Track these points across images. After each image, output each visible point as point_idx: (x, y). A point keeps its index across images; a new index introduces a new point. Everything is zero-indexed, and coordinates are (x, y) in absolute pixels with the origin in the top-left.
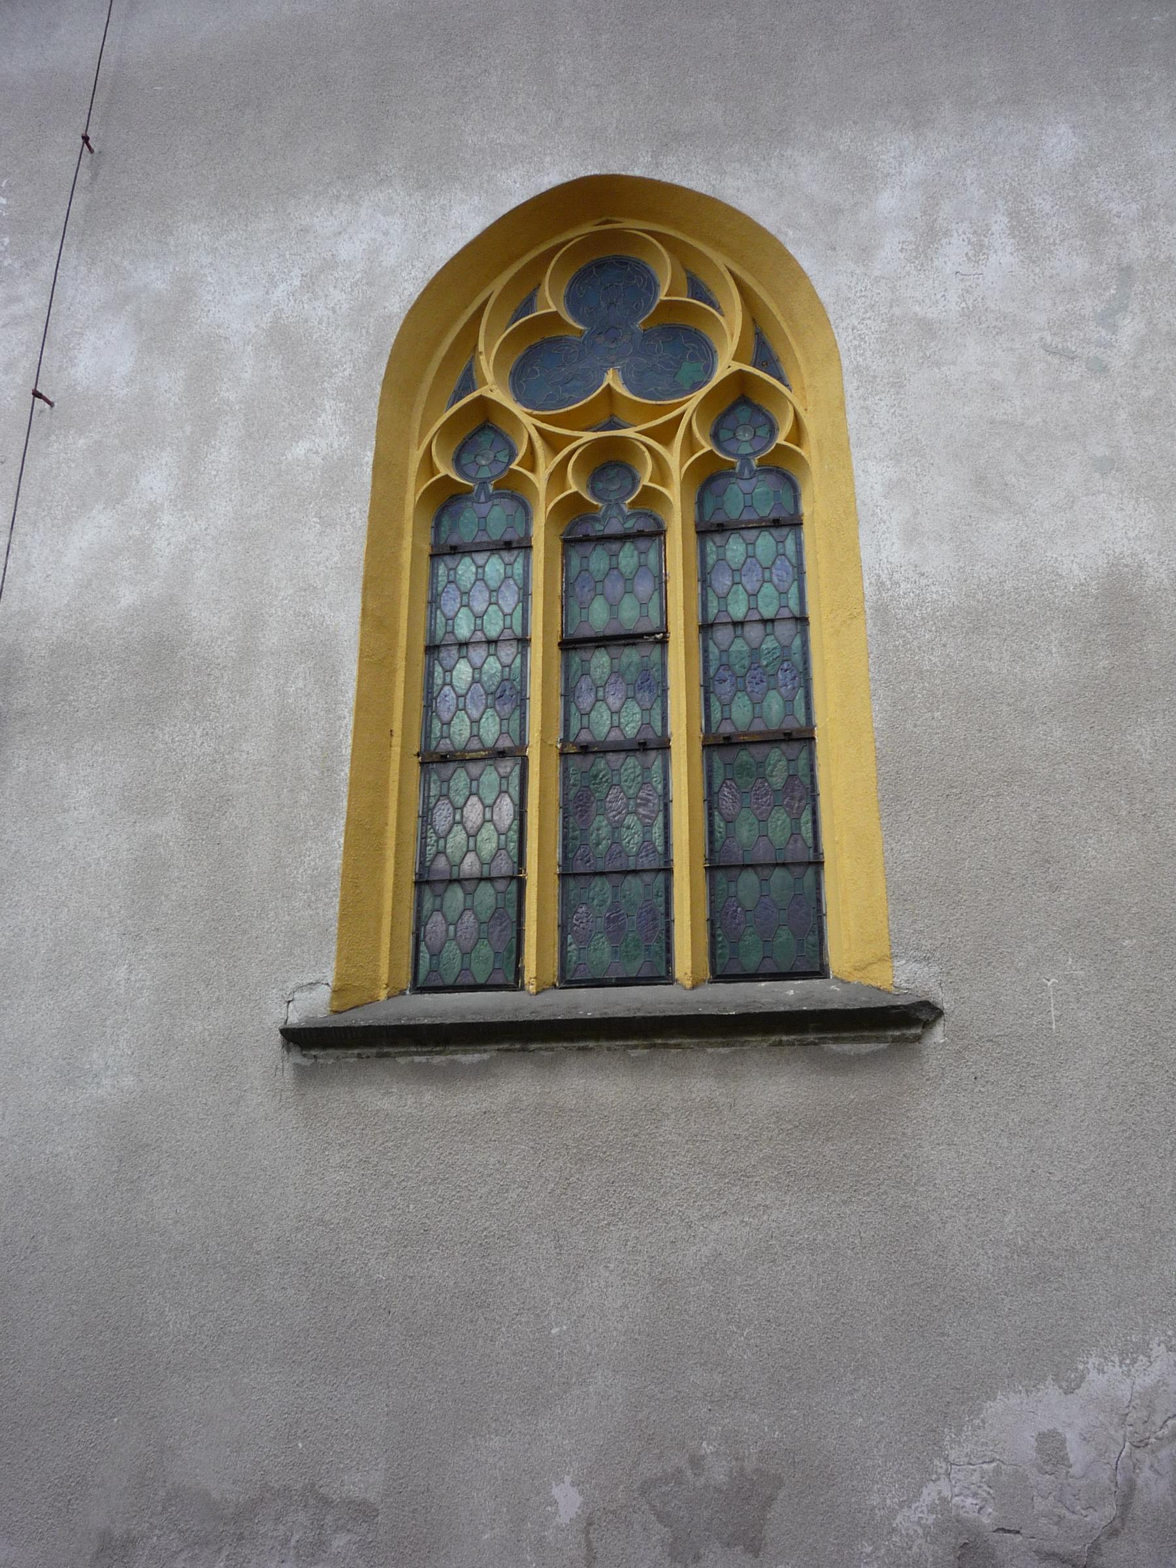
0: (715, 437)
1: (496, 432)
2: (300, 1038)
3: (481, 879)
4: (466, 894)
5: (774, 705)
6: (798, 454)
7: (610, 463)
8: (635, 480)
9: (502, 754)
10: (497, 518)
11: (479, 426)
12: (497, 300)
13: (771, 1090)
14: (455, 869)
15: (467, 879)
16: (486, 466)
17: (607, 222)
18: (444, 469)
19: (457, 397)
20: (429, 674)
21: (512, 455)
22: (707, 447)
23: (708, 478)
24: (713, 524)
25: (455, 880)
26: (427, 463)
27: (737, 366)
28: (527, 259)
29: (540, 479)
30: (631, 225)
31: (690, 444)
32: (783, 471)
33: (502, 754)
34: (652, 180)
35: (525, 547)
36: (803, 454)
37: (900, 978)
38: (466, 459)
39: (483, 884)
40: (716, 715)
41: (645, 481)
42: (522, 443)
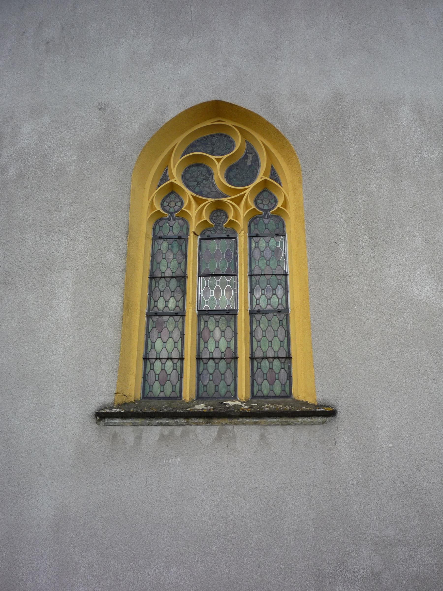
0: (256, 203)
1: (269, 192)
2: (102, 416)
3: (275, 358)
4: (270, 363)
5: (172, 304)
6: (285, 212)
7: (219, 210)
9: (177, 314)
11: (172, 192)
13: (282, 437)
14: (158, 355)
15: (216, 358)
16: (173, 207)
17: (219, 121)
18: (158, 208)
22: (253, 207)
23: (253, 219)
25: (276, 358)
27: (264, 178)
30: (229, 123)
31: (247, 206)
33: (279, 312)
34: (242, 108)
36: (287, 211)
39: (222, 360)
40: (254, 303)
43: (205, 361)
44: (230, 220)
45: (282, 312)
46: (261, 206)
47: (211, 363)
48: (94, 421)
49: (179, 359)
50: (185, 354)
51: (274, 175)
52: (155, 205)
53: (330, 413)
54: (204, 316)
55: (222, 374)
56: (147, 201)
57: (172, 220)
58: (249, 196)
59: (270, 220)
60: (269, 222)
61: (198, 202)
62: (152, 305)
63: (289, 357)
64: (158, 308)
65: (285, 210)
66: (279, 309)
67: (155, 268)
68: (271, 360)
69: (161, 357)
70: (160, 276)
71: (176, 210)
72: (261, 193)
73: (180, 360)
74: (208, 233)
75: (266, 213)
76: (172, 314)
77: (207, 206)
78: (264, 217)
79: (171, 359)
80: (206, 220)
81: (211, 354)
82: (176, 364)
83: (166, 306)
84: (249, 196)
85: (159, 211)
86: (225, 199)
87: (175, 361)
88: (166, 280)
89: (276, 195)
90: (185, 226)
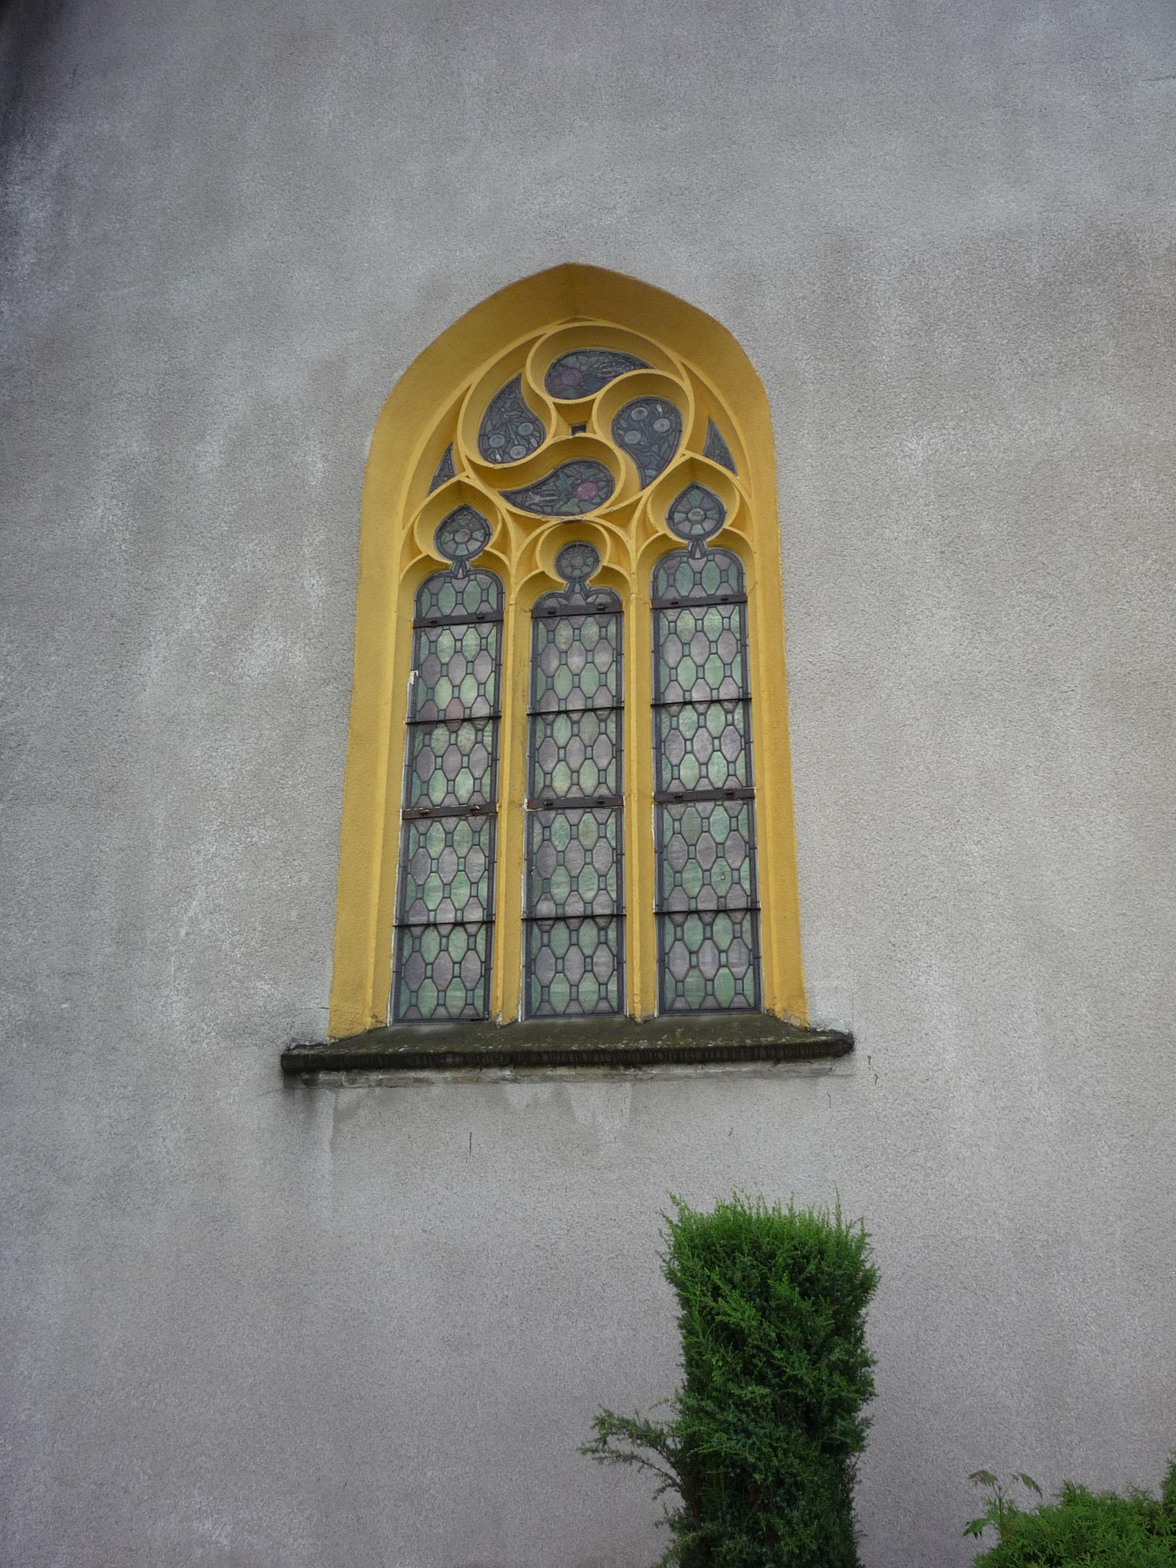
8: (597, 560)
10: (475, 594)
12: (547, 340)
18: (428, 548)
19: (434, 486)
20: (658, 728)
21: (488, 535)
23: (664, 556)
24: (667, 600)
26: (411, 545)
27: (690, 454)
28: (504, 352)
29: (512, 560)
31: (645, 527)
32: (731, 548)
35: (498, 620)
37: (826, 1011)
38: (447, 537)
40: (666, 775)
41: (605, 563)
42: (619, 475)
43: (679, 918)
44: (604, 567)
45: (737, 794)
46: (685, 527)
47: (693, 924)
48: (278, 1083)
49: (483, 923)
50: (626, 901)
51: (718, 449)
52: (419, 544)
53: (838, 1047)
54: (669, 806)
55: (454, 963)
56: (398, 534)
57: (460, 576)
58: (649, 506)
59: (708, 561)
60: (709, 568)
61: (527, 525)
62: (539, 786)
63: (753, 910)
64: (581, 789)
65: (501, 556)
66: (601, 797)
67: (664, 680)
68: (707, 918)
69: (465, 920)
70: (556, 709)
71: (707, 529)
72: (452, 517)
73: (484, 926)
74: (551, 603)
75: (698, 545)
76: (466, 811)
77: (543, 537)
78: (691, 555)
79: (726, 911)
80: (543, 573)
81: (589, 907)
82: (475, 936)
83: (451, 792)
84: (649, 506)
85: (664, 536)
86: (589, 517)
87: (472, 929)
88: (570, 719)
89: (723, 500)
90: (733, 572)
